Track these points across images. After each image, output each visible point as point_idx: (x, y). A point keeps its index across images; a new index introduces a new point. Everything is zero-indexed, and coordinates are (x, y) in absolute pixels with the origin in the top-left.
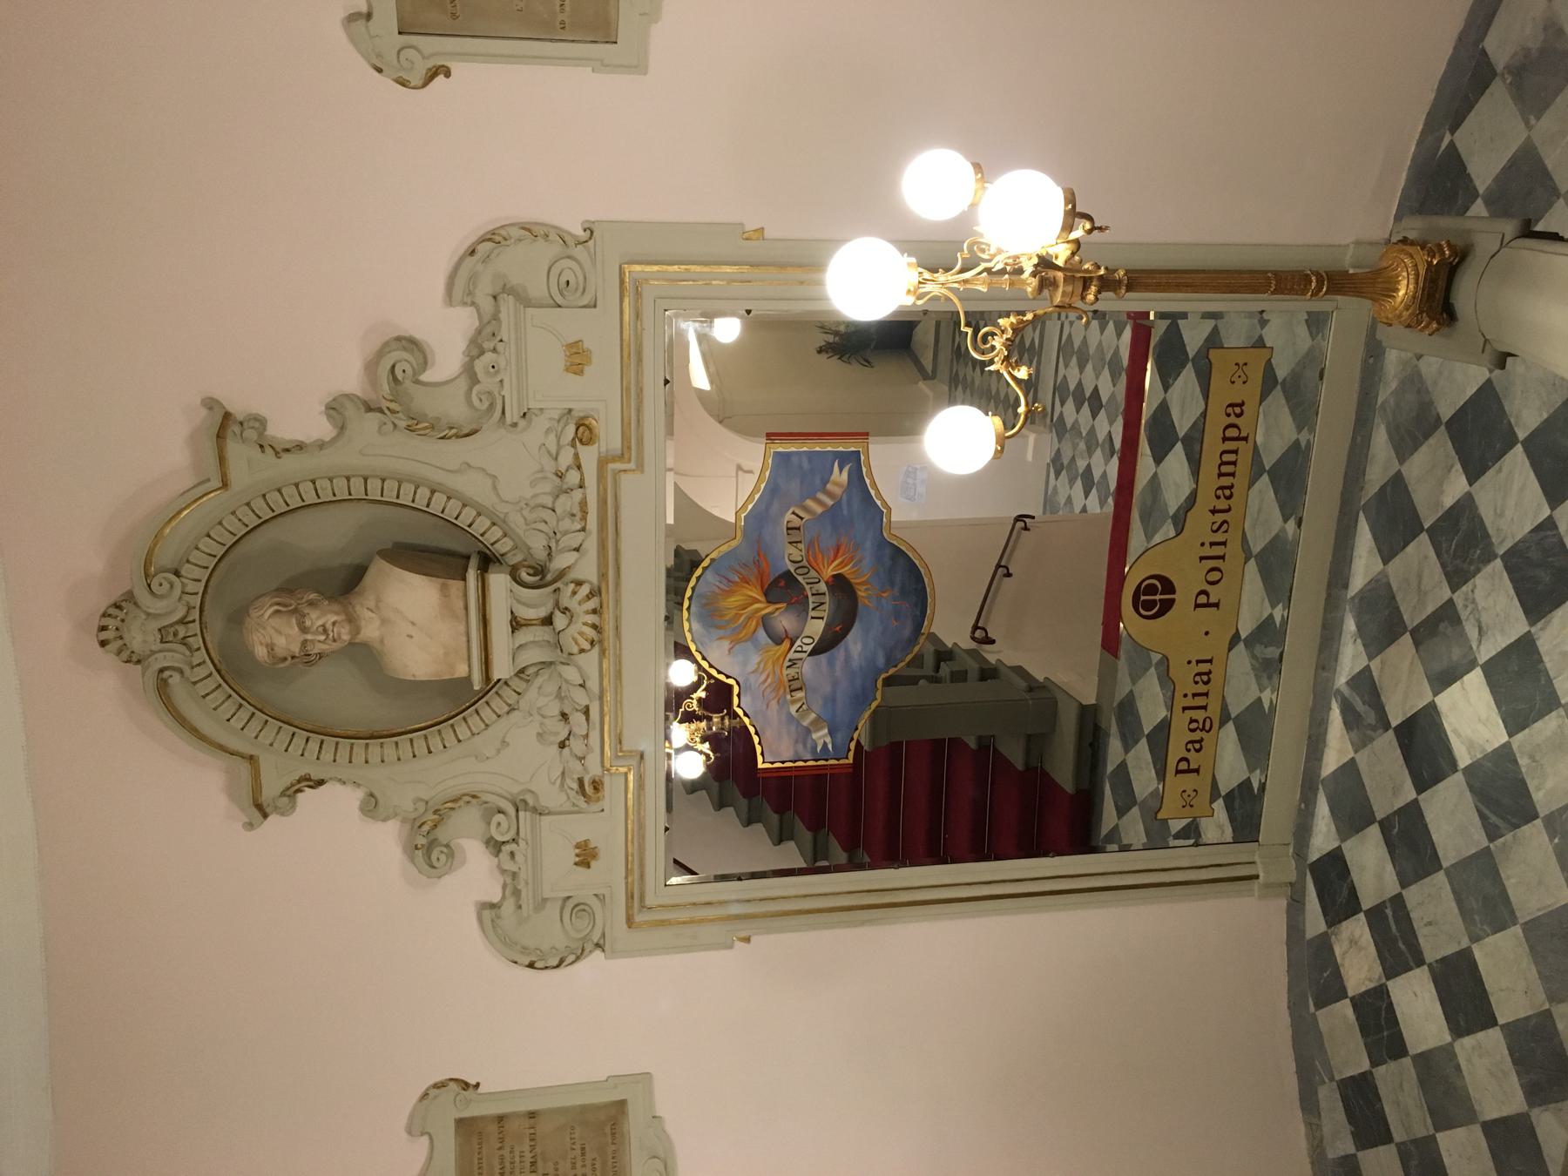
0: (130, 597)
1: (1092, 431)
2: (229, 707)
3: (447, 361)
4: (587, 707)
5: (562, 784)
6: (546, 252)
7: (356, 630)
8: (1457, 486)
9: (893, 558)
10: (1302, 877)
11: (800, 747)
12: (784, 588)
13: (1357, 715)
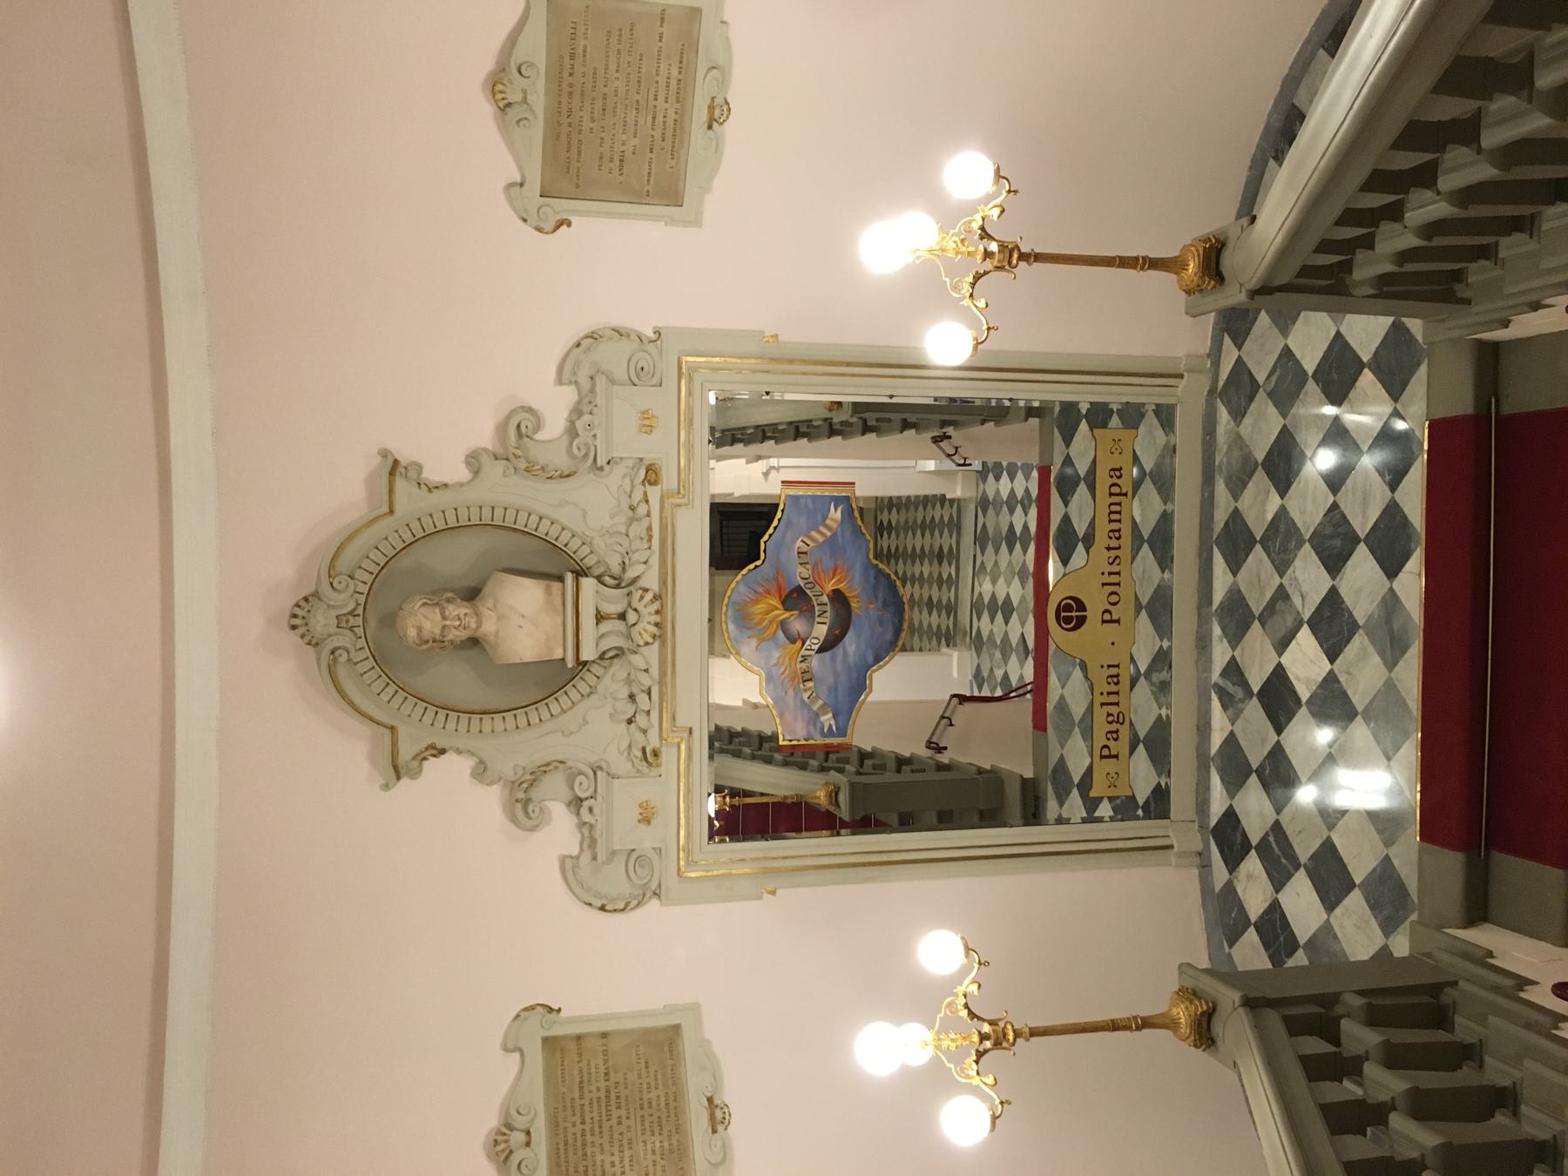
0: (316, 594)
2: (380, 684)
3: (554, 425)
6: (627, 347)
8: (1274, 502)
10: (1207, 845)
12: (796, 599)
13: (1231, 696)
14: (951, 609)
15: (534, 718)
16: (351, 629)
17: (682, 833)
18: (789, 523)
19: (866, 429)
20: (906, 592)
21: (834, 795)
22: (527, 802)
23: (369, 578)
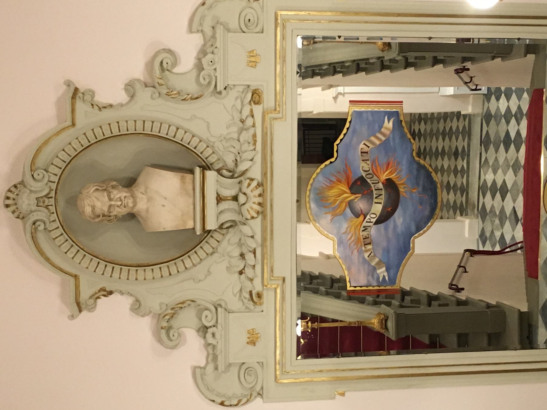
0: (22, 183)
1: (502, 210)
3: (187, 62)
4: (255, 250)
5: (240, 296)
7: (135, 203)
9: (418, 170)
11: (370, 278)
12: (359, 186)
14: (464, 190)
15: (174, 270)
16: (47, 207)
17: (278, 352)
18: (354, 131)
19: (408, 65)
20: (437, 178)
21: (384, 321)
22: (168, 329)
23: (58, 172)
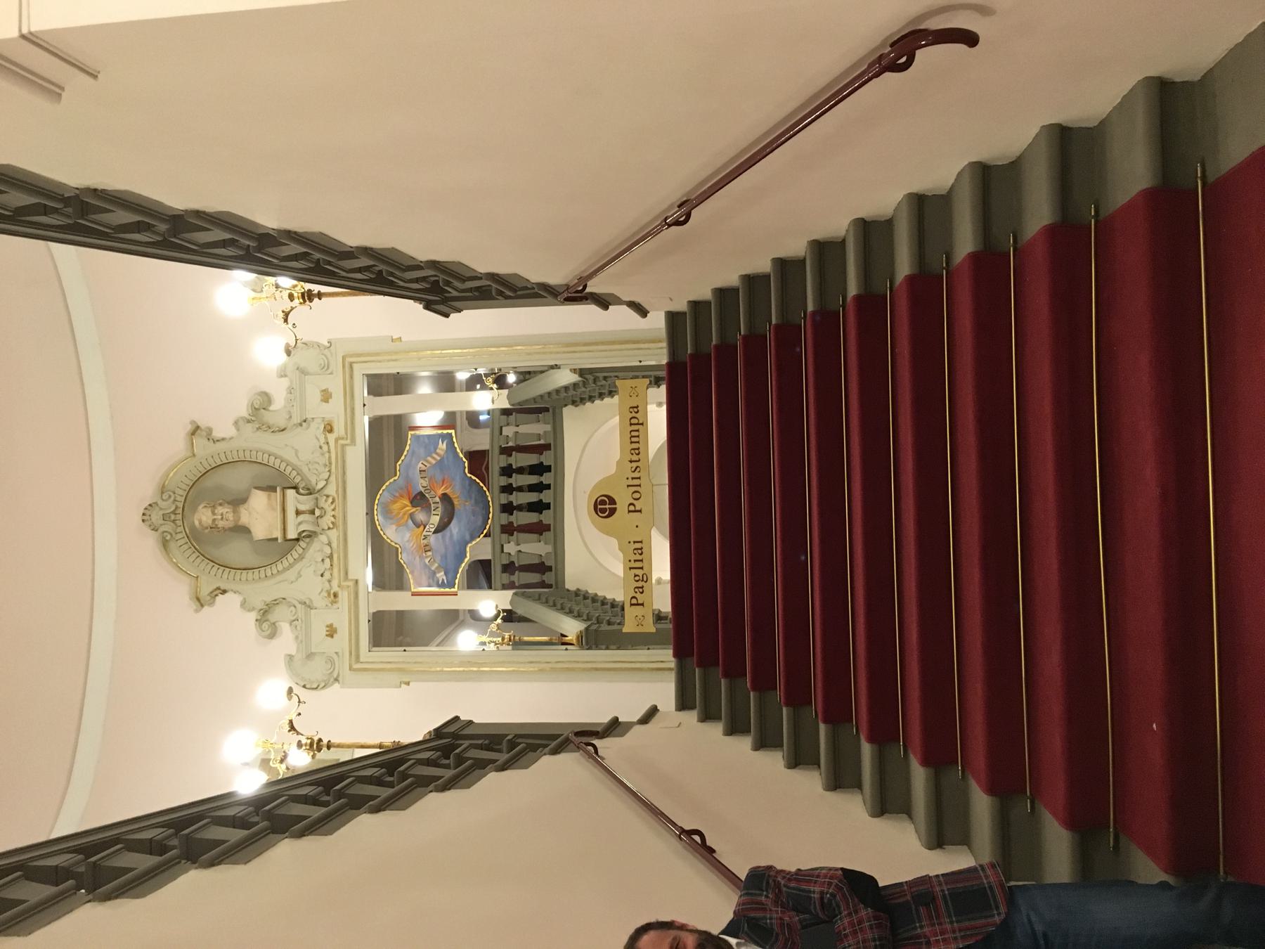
2: (190, 552)
12: (419, 500)
16: (174, 521)
18: (413, 453)
